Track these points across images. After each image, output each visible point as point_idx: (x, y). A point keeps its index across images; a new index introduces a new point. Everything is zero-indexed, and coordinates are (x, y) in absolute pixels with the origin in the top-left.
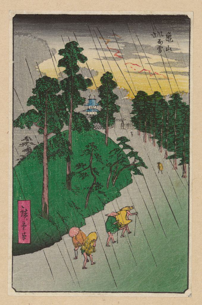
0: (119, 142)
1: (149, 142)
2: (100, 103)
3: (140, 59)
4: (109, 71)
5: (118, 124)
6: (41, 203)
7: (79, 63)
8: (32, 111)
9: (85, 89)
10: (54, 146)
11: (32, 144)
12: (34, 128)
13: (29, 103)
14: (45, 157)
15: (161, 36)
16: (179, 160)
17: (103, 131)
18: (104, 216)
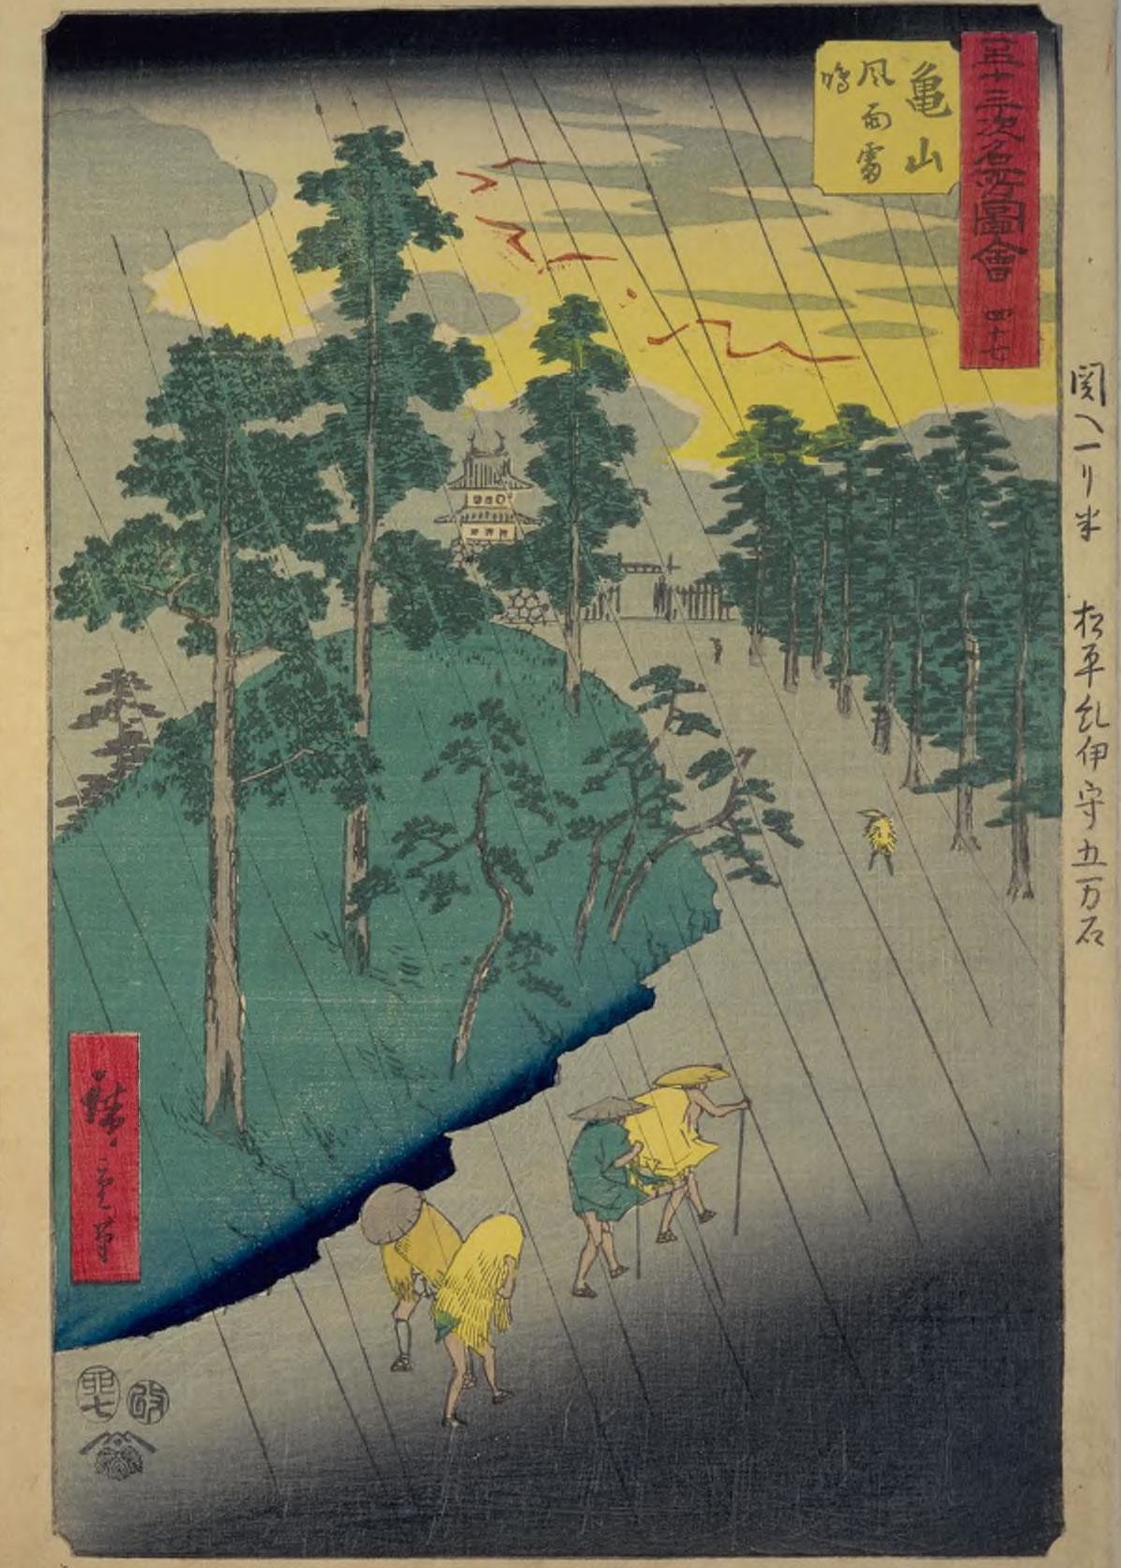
0: (647, 694)
1: (816, 691)
2: (537, 472)
3: (756, 222)
4: (629, 529)
5: (637, 592)
6: (199, 1047)
7: (414, 256)
8: (152, 519)
9: (446, 398)
10: (270, 718)
11: (148, 710)
12: (166, 624)
13: (133, 480)
14: (222, 782)
15: (881, 82)
16: (989, 799)
17: (551, 633)
18: (563, 1123)
